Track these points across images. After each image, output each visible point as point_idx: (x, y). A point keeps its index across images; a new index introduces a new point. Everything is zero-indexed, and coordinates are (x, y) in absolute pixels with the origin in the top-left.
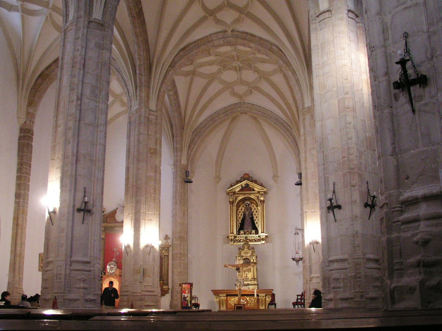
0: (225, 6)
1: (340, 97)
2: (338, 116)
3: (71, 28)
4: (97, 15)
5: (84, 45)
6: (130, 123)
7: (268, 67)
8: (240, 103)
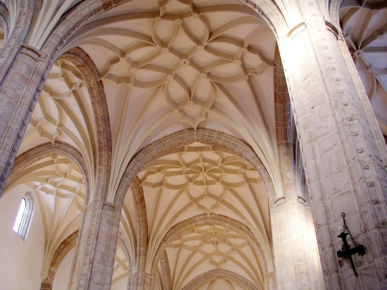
0: (206, 196)
1: (295, 264)
2: (295, 280)
3: (90, 208)
4: (110, 199)
5: (99, 222)
6: (129, 284)
7: (238, 242)
8: (217, 269)
